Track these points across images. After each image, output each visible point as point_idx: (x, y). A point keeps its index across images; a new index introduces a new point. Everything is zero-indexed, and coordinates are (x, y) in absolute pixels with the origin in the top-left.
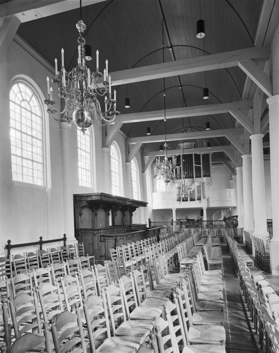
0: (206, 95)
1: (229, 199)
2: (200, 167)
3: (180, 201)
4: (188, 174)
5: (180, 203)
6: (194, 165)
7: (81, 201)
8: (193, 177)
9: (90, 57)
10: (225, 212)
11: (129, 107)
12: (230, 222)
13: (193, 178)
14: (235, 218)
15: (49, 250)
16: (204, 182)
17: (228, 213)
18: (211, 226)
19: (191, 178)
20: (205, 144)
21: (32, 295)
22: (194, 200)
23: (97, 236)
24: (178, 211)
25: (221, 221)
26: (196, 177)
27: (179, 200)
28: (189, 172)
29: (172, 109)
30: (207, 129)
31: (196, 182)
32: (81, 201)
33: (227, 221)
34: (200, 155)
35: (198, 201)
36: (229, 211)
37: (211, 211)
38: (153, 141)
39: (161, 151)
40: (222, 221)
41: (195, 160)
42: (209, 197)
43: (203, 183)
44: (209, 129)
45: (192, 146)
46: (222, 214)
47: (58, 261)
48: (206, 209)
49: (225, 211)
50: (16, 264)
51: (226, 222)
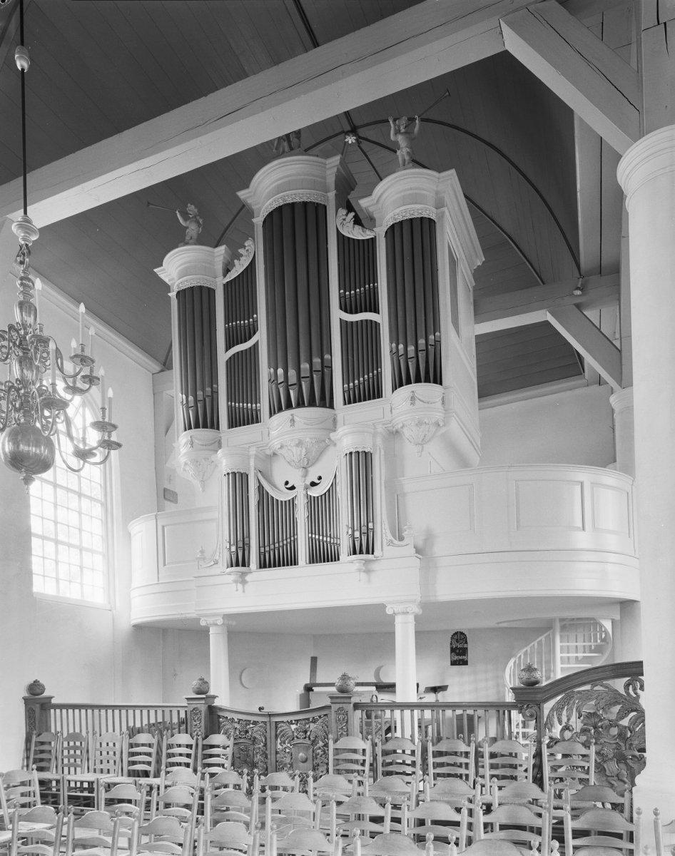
2: (374, 326)
4: (293, 378)
6: (337, 315)
10: (580, 644)
14: (619, 684)
33: (548, 706)
36: (603, 640)
40: (510, 706)
41: (342, 285)
43: (394, 434)
46: (558, 655)
49: (580, 638)
50: (337, 814)
51: (537, 717)
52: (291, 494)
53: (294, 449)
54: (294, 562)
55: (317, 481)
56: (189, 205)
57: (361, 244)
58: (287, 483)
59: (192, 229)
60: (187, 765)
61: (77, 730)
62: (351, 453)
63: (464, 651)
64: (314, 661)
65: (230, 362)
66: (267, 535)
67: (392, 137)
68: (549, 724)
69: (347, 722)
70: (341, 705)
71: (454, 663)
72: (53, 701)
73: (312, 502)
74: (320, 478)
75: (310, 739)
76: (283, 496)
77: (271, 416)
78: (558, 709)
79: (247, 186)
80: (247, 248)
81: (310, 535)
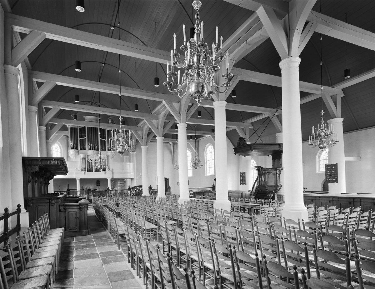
0: (157, 83)
1: (129, 171)
3: (85, 171)
5: (85, 174)
7: (31, 165)
8: (98, 150)
9: (83, 8)
11: (80, 71)
12: (134, 191)
13: (98, 150)
15: (281, 214)
16: (109, 155)
17: (123, 183)
18: (92, 195)
19: (96, 150)
20: (110, 121)
21: (238, 261)
23: (55, 206)
24: (83, 181)
25: (126, 190)
26: (80, 150)
27: (84, 170)
28: (94, 144)
30: (136, 110)
31: (81, 153)
32: (31, 165)
34: (105, 130)
35: (104, 172)
37: (114, 180)
38: (64, 108)
39: (75, 120)
40: (127, 190)
42: (114, 169)
43: (108, 156)
44: (137, 110)
45: (98, 121)
46: (118, 184)
47: (238, 210)
48: (79, 180)
52: (92, 161)
54: (92, 171)
57: (91, 129)
60: (268, 204)
64: (68, 185)
65: (80, 140)
68: (132, 191)
71: (97, 185)
72: (153, 188)
76: (91, 162)
78: (133, 190)
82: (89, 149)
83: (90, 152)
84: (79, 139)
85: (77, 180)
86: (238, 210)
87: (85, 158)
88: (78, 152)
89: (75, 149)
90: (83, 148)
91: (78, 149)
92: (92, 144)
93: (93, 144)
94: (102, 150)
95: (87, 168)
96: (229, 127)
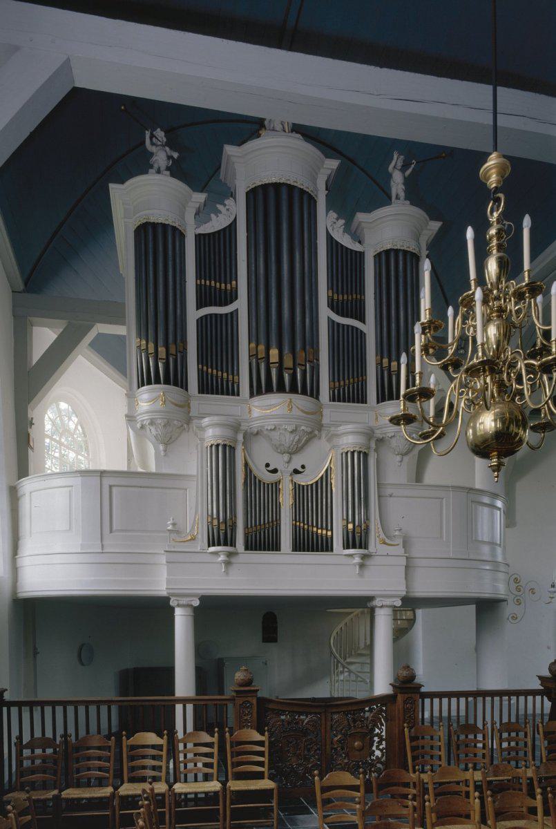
2: (362, 335)
3: (233, 544)
8: (315, 393)
22: (324, 545)
24: (214, 613)
26: (333, 399)
27: (221, 536)
29: (506, 89)
41: (331, 286)
47: (261, 759)
48: (189, 612)
53: (288, 435)
54: (275, 546)
55: (301, 470)
56: (159, 130)
58: (267, 465)
59: (161, 157)
61: (471, 721)
62: (218, 446)
63: (275, 630)
65: (201, 322)
66: (249, 517)
67: (391, 168)
69: (414, 711)
70: (410, 695)
73: (299, 490)
74: (303, 467)
75: (368, 728)
76: (268, 478)
77: (139, 387)
79: (241, 143)
80: (227, 207)
81: (294, 522)
82: (258, 389)
83: (268, 411)
84: (193, 314)
85: (179, 612)
86: (261, 759)
87: (233, 449)
88: (185, 406)
89: (167, 382)
90: (217, 383)
91: (184, 385)
92: (227, 372)
93: (286, 350)
94: (338, 396)
95: (246, 527)
96: (246, 465)
